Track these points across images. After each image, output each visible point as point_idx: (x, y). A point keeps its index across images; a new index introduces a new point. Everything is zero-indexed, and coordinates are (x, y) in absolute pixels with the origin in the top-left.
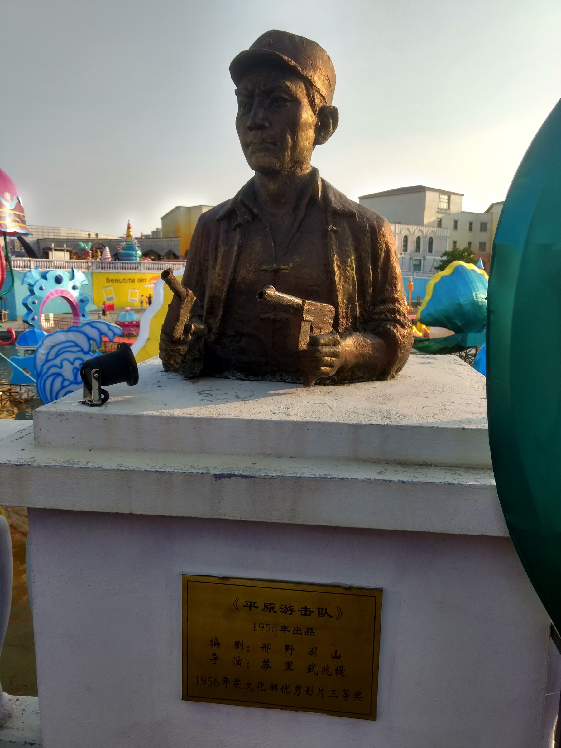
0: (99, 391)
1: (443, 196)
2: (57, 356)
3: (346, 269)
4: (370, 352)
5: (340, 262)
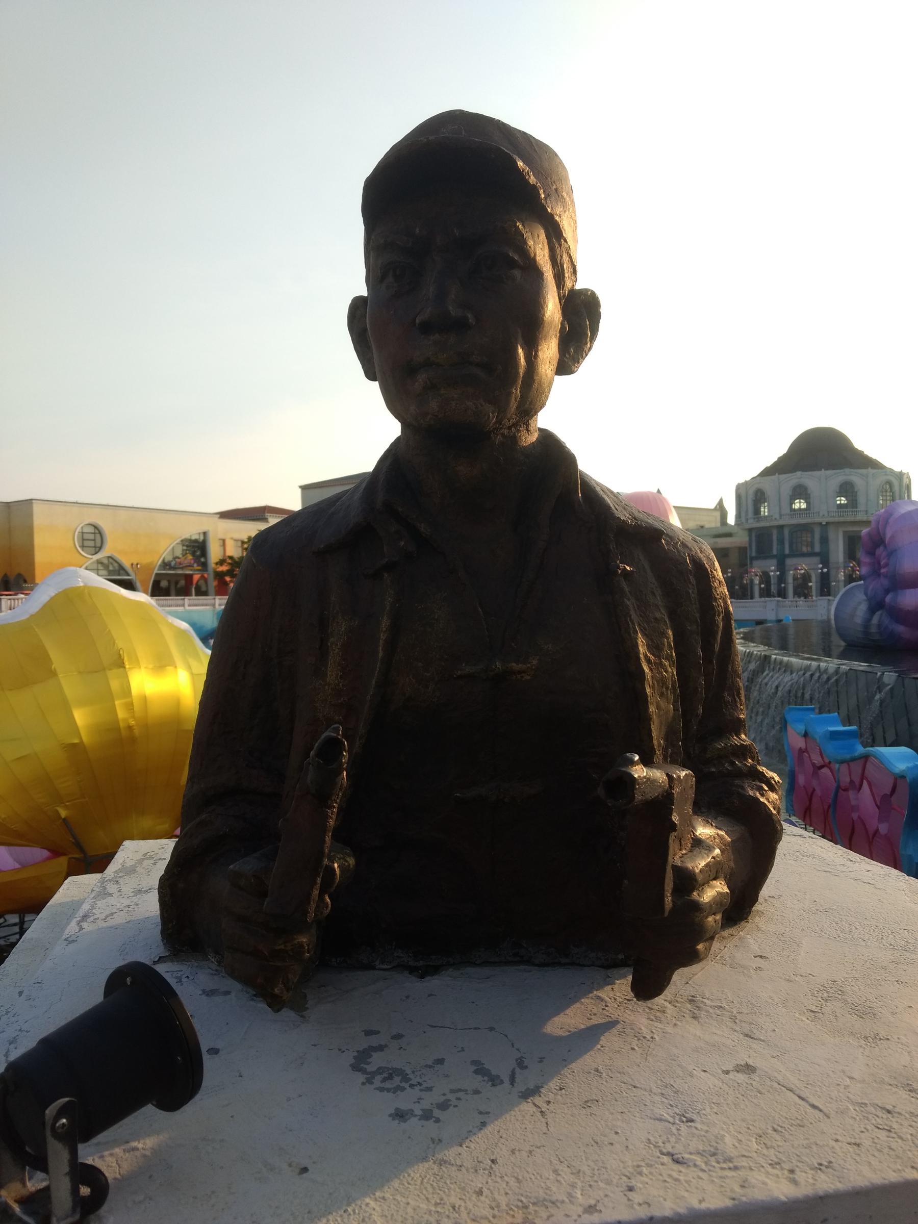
0: (74, 1201)
3: (661, 665)
4: (732, 864)
5: (649, 648)
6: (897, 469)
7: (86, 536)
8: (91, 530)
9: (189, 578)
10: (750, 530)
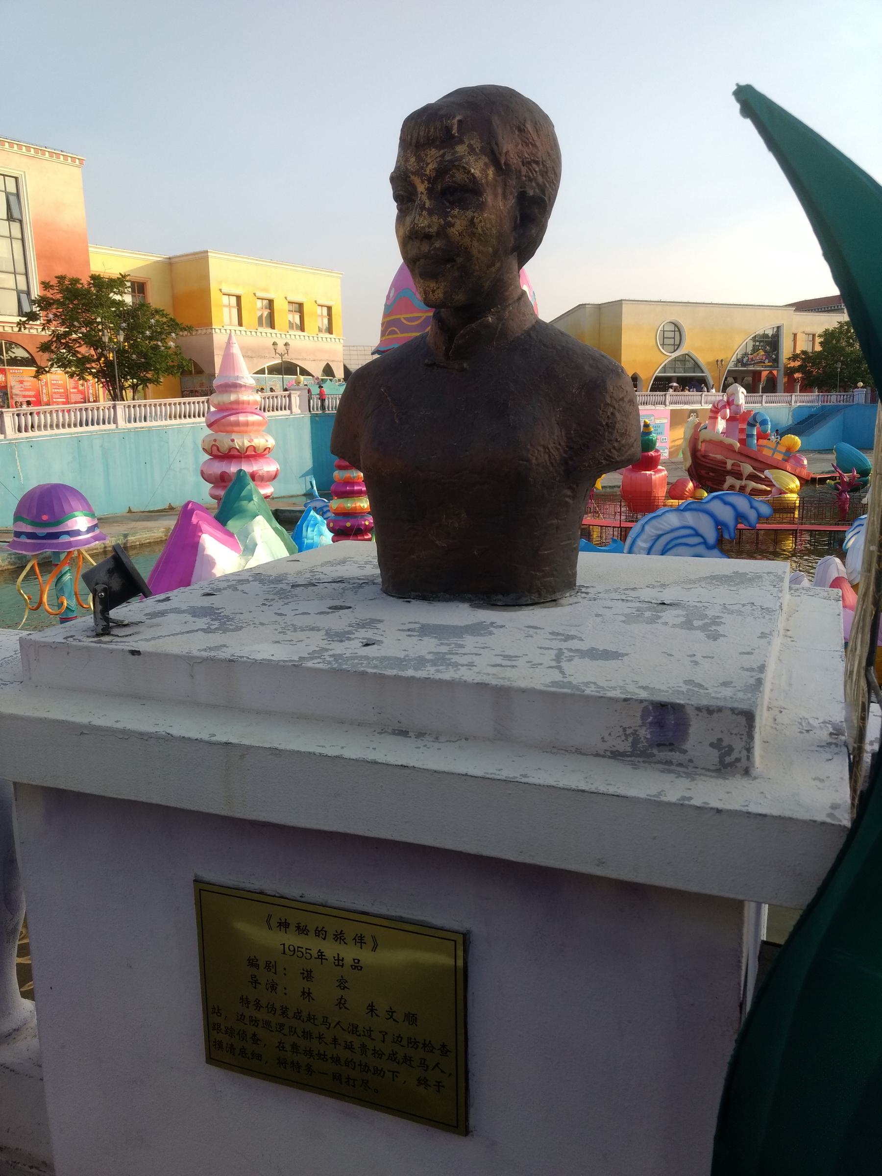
7: (667, 335)
8: (672, 328)
9: (757, 375)
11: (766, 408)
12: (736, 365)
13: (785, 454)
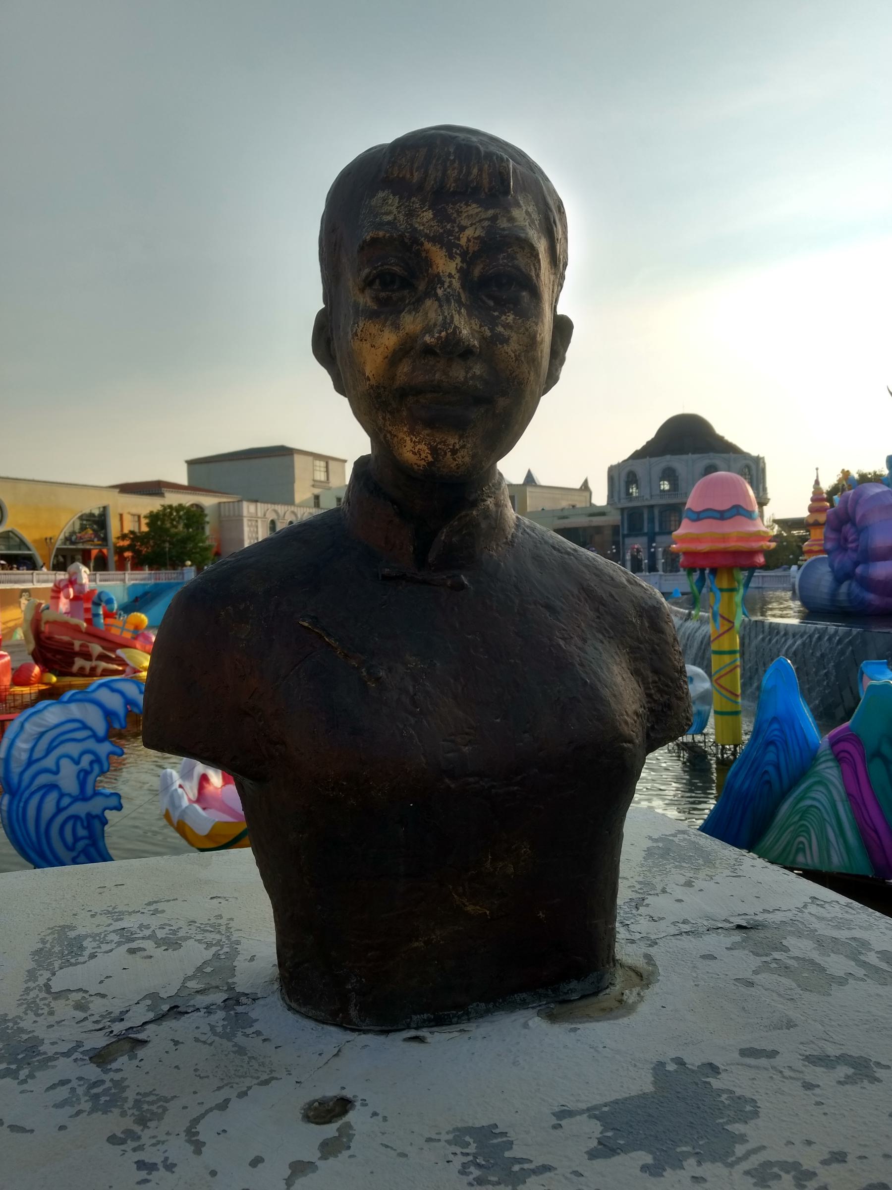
1: (317, 463)
2: (49, 751)
6: (754, 453)
10: (622, 510)
11: (101, 586)
12: (64, 543)
13: (133, 632)
